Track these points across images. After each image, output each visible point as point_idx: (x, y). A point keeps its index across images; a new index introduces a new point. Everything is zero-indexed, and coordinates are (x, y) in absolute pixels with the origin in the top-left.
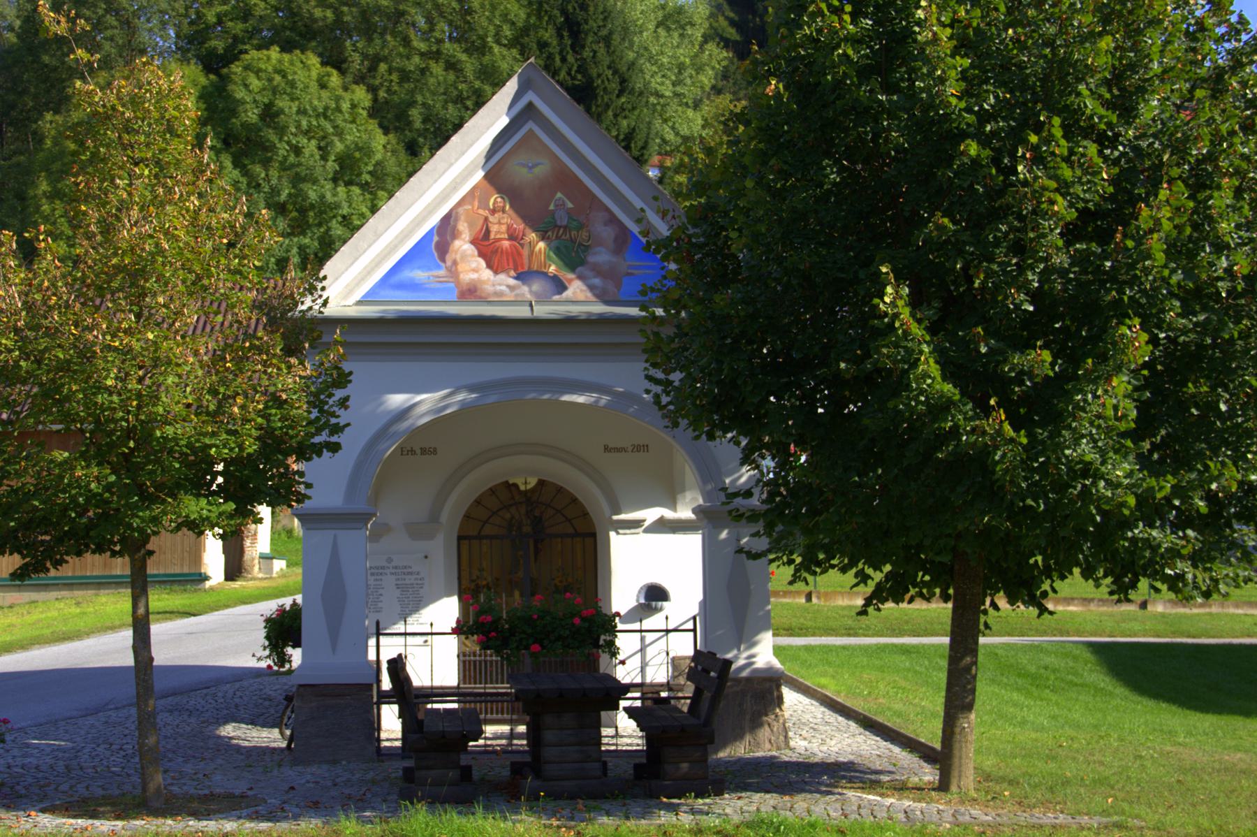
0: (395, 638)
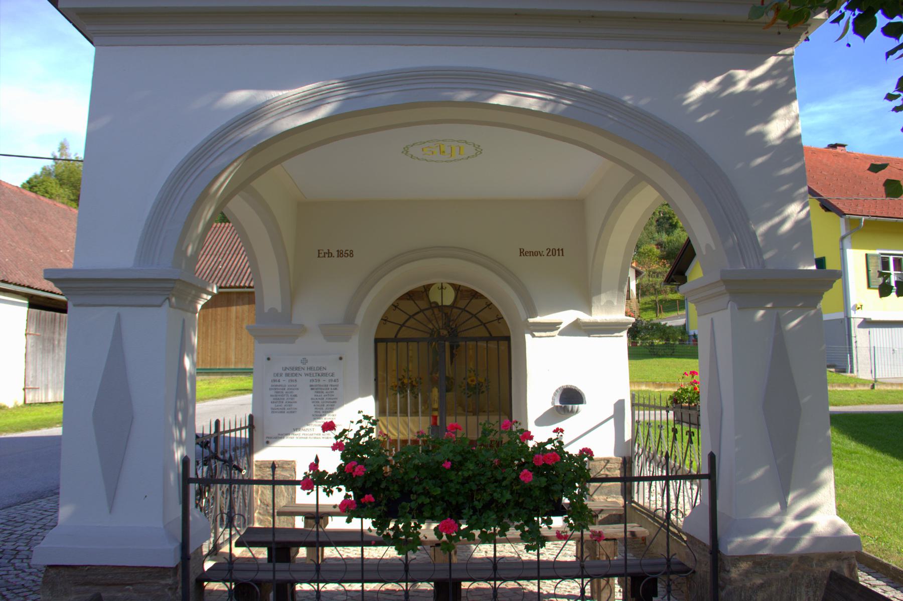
0: (177, 511)
